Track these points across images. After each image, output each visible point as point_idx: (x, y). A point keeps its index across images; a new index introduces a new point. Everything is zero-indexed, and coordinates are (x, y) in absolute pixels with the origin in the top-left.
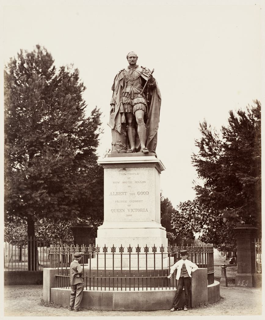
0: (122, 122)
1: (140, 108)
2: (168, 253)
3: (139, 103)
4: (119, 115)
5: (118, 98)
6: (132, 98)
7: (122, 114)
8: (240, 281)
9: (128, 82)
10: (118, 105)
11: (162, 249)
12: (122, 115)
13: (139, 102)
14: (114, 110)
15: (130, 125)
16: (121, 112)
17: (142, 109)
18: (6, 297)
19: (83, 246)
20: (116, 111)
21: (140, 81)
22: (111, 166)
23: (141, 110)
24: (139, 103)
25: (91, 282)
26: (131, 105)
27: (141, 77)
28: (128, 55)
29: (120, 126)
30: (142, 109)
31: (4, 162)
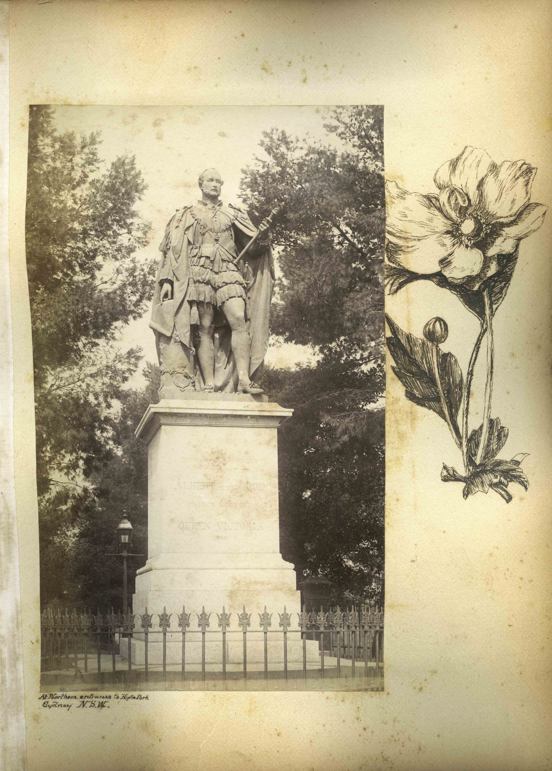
0: (192, 323)
1: (239, 295)
2: (300, 629)
3: (235, 283)
4: (186, 305)
5: (184, 268)
6: (216, 270)
7: (191, 303)
8: (80, 403)
9: (207, 234)
10: (183, 283)
11: (285, 620)
12: (191, 308)
13: (235, 281)
14: (170, 293)
15: (206, 331)
16: (190, 299)
17: (241, 296)
18: (305, 81)
19: (111, 613)
20: (179, 296)
21: (231, 235)
22: (231, 422)
23: (241, 299)
24: (235, 283)
25: (127, 643)
26: (212, 287)
27: (234, 225)
28: (204, 175)
29: (186, 330)
30: (241, 296)
31: (35, 396)
